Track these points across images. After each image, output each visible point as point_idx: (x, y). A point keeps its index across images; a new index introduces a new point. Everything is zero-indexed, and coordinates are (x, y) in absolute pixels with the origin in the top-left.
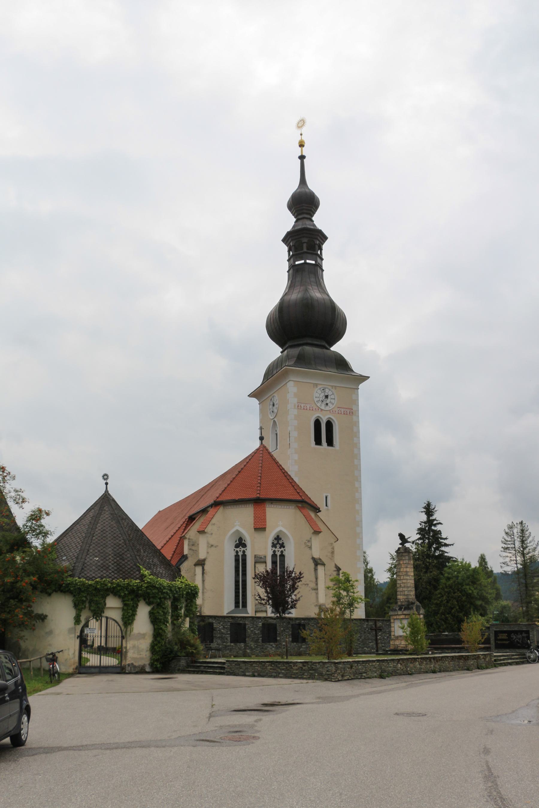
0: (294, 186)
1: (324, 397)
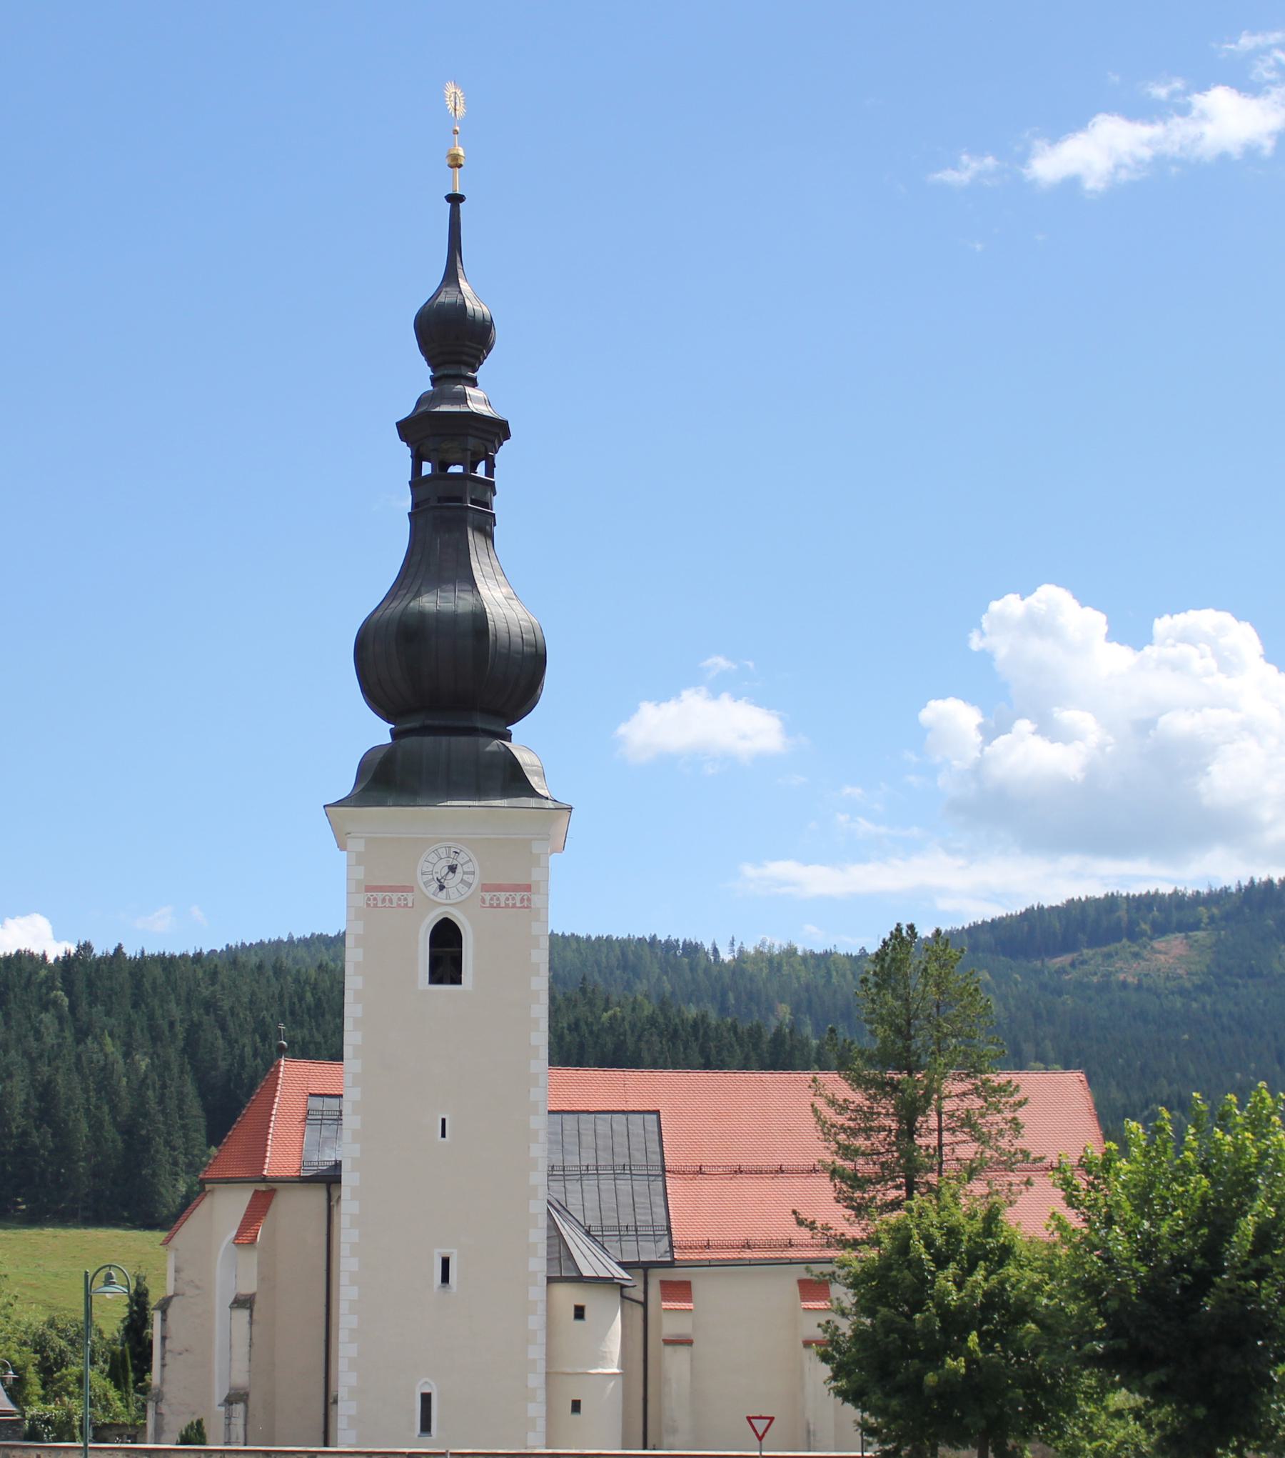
0: (423, 286)
1: (446, 869)
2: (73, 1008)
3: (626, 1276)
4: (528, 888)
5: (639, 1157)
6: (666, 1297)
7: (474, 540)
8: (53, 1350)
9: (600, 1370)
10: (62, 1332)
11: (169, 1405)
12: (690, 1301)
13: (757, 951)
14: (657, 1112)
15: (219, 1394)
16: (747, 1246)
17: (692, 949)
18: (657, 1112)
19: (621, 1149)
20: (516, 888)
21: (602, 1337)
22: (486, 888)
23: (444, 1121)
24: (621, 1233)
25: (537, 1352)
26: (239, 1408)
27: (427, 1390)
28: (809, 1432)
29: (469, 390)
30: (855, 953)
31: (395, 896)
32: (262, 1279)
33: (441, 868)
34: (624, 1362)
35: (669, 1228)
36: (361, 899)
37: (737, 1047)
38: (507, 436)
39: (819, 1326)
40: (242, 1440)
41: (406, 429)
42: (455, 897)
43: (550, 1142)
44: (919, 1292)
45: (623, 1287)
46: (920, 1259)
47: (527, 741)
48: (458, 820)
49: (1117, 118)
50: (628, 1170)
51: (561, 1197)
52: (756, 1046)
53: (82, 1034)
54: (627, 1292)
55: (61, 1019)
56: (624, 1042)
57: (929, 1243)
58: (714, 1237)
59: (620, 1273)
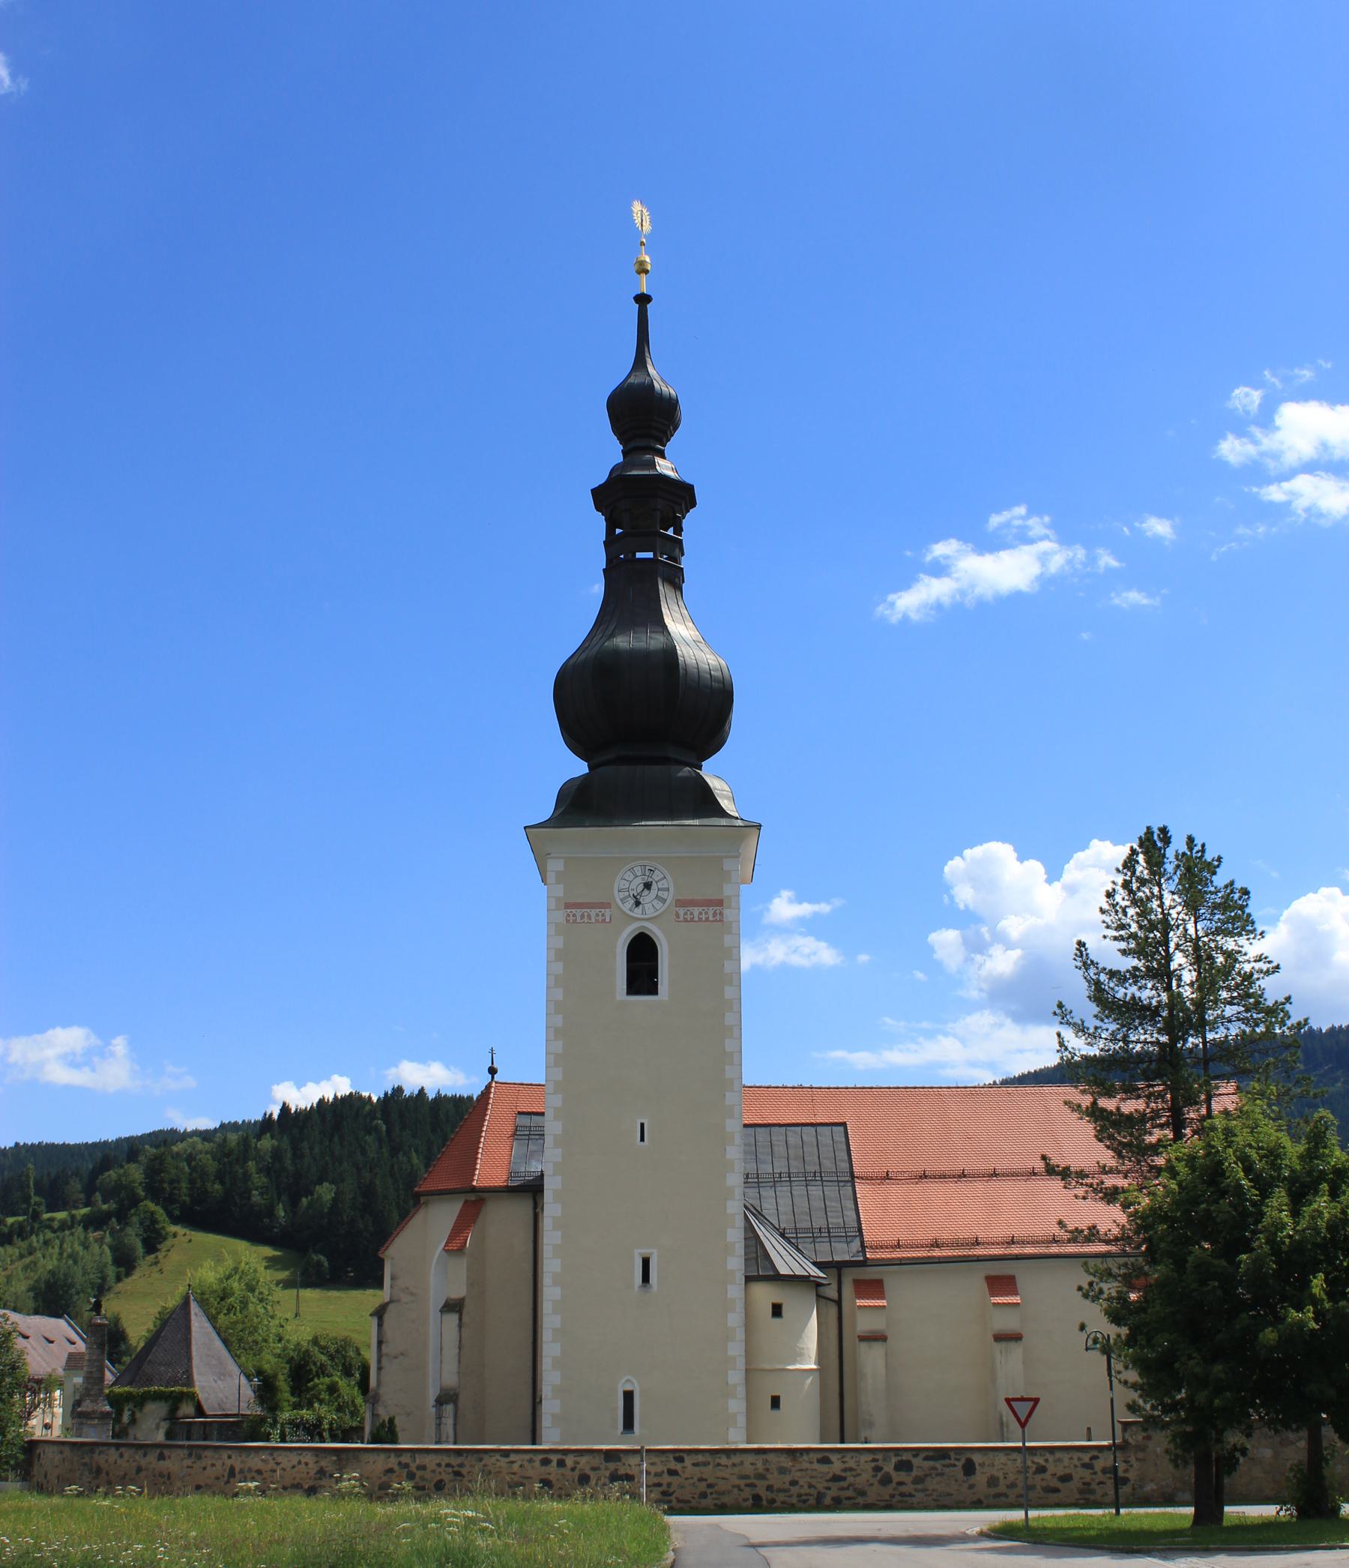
0: (617, 371)
1: (641, 887)
2: (389, 1131)
3: (822, 1275)
4: (720, 903)
5: (828, 1165)
6: (860, 1295)
7: (664, 590)
8: (315, 1364)
9: (798, 1366)
10: (323, 1349)
12: (883, 1298)
14: (844, 1124)
15: (432, 1394)
16: (936, 1244)
18: (844, 1124)
19: (812, 1158)
20: (709, 903)
21: (799, 1334)
22: (680, 903)
23: (642, 1125)
24: (815, 1235)
25: (736, 1349)
26: (449, 1408)
27: (629, 1388)
28: (1002, 1424)
29: (658, 460)
31: (593, 912)
32: (471, 1284)
33: (637, 885)
34: (821, 1358)
35: (860, 1230)
36: (560, 916)
38: (693, 504)
39: (1080, 1289)
40: (451, 1439)
41: (601, 496)
42: (650, 913)
43: (745, 1152)
44: (1237, 1229)
45: (818, 1285)
46: (1241, 1186)
47: (716, 774)
48: (653, 835)
50: (818, 1177)
51: (756, 1203)
53: (395, 1150)
54: (823, 1290)
55: (380, 1140)
57: (1248, 1169)
58: (904, 1237)
59: (815, 1271)
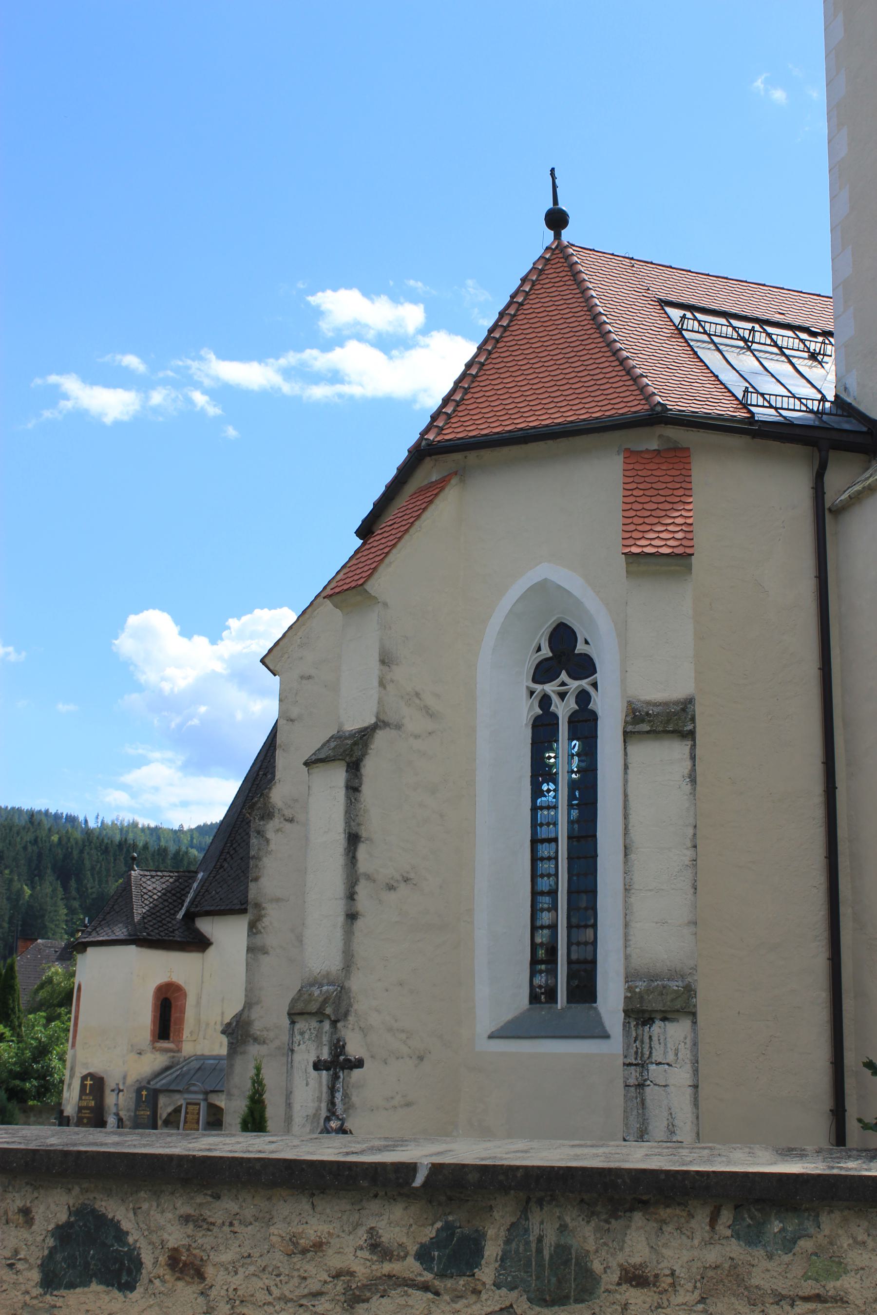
11: (364, 1031)
13: (113, 823)
17: (72, 820)
26: (672, 1035)
30: (176, 828)
37: (150, 861)
49: (255, 387)
52: (164, 860)
56: (71, 853)
